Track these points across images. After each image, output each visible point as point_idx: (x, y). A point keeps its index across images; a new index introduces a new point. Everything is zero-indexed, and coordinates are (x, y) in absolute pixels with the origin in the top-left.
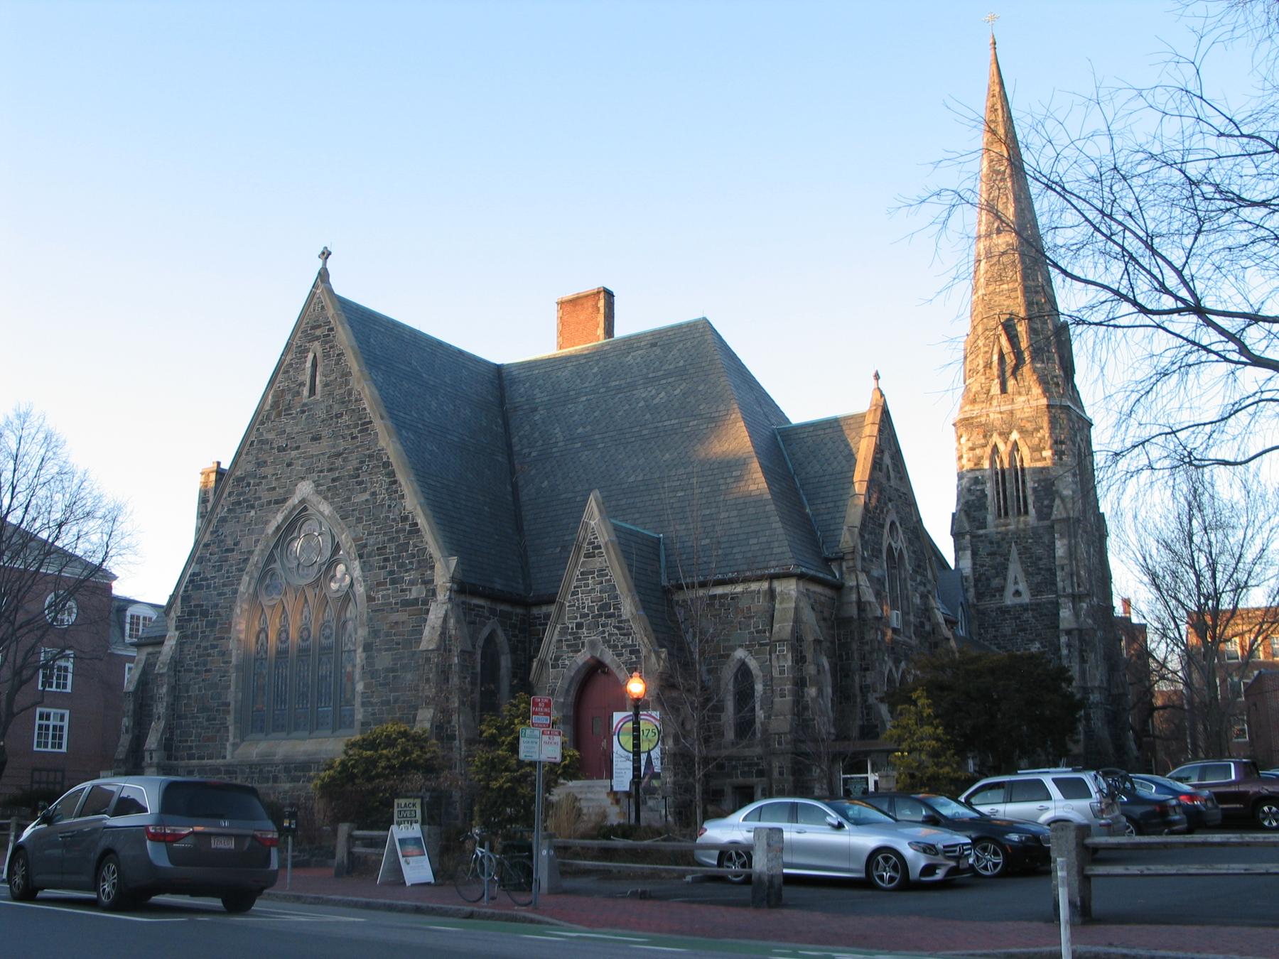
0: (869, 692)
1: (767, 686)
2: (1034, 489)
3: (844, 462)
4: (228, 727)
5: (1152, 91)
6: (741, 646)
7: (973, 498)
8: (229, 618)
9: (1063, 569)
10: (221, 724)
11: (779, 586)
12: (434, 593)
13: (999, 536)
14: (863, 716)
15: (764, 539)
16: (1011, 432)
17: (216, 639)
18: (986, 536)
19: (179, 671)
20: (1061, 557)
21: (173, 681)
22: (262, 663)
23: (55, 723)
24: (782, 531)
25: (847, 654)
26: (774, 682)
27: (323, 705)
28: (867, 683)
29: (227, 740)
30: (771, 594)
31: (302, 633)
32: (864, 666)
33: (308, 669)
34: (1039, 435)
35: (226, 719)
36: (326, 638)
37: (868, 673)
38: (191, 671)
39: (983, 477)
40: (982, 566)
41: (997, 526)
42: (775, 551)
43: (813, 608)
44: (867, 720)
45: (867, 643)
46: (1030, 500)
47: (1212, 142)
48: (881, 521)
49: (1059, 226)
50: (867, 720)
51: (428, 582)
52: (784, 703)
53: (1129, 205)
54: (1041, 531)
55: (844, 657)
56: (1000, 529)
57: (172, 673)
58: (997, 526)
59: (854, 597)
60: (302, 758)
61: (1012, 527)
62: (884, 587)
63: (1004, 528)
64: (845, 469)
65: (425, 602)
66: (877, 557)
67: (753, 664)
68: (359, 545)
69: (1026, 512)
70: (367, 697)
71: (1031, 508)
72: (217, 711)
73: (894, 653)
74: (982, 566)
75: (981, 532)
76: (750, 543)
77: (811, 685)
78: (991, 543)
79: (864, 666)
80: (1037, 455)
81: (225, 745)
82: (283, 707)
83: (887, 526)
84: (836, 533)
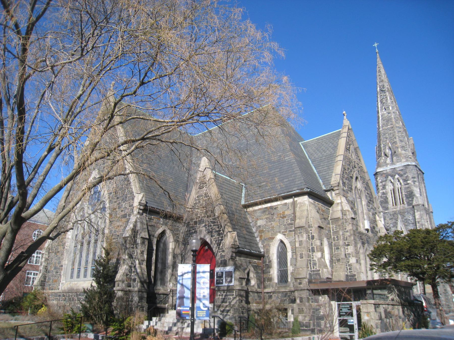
0: (350, 257)
1: (294, 253)
2: (405, 195)
3: (332, 150)
6: (280, 232)
7: (382, 199)
9: (419, 223)
11: (299, 200)
13: (393, 212)
14: (347, 270)
15: (291, 179)
16: (395, 175)
18: (389, 213)
20: (418, 219)
21: (47, 257)
23: (31, 276)
24: (300, 174)
25: (337, 237)
26: (297, 250)
28: (349, 252)
29: (61, 282)
30: (294, 203)
32: (346, 244)
34: (406, 175)
37: (349, 247)
39: (386, 192)
40: (388, 223)
41: (393, 209)
42: (297, 183)
43: (318, 212)
44: (350, 272)
45: (347, 231)
46: (404, 199)
48: (351, 175)
50: (350, 272)
51: (131, 206)
52: (301, 263)
54: (409, 210)
55: (336, 239)
56: (393, 210)
57: (47, 253)
58: (393, 209)
59: (339, 208)
61: (398, 209)
62: (355, 206)
63: (395, 209)
64: (333, 153)
66: (351, 192)
67: (286, 242)
69: (403, 203)
71: (405, 201)
73: (362, 239)
74: (388, 223)
75: (386, 211)
76: (284, 181)
77: (318, 251)
78: (391, 215)
79: (346, 244)
80: (405, 183)
83: (354, 178)
84: (329, 179)
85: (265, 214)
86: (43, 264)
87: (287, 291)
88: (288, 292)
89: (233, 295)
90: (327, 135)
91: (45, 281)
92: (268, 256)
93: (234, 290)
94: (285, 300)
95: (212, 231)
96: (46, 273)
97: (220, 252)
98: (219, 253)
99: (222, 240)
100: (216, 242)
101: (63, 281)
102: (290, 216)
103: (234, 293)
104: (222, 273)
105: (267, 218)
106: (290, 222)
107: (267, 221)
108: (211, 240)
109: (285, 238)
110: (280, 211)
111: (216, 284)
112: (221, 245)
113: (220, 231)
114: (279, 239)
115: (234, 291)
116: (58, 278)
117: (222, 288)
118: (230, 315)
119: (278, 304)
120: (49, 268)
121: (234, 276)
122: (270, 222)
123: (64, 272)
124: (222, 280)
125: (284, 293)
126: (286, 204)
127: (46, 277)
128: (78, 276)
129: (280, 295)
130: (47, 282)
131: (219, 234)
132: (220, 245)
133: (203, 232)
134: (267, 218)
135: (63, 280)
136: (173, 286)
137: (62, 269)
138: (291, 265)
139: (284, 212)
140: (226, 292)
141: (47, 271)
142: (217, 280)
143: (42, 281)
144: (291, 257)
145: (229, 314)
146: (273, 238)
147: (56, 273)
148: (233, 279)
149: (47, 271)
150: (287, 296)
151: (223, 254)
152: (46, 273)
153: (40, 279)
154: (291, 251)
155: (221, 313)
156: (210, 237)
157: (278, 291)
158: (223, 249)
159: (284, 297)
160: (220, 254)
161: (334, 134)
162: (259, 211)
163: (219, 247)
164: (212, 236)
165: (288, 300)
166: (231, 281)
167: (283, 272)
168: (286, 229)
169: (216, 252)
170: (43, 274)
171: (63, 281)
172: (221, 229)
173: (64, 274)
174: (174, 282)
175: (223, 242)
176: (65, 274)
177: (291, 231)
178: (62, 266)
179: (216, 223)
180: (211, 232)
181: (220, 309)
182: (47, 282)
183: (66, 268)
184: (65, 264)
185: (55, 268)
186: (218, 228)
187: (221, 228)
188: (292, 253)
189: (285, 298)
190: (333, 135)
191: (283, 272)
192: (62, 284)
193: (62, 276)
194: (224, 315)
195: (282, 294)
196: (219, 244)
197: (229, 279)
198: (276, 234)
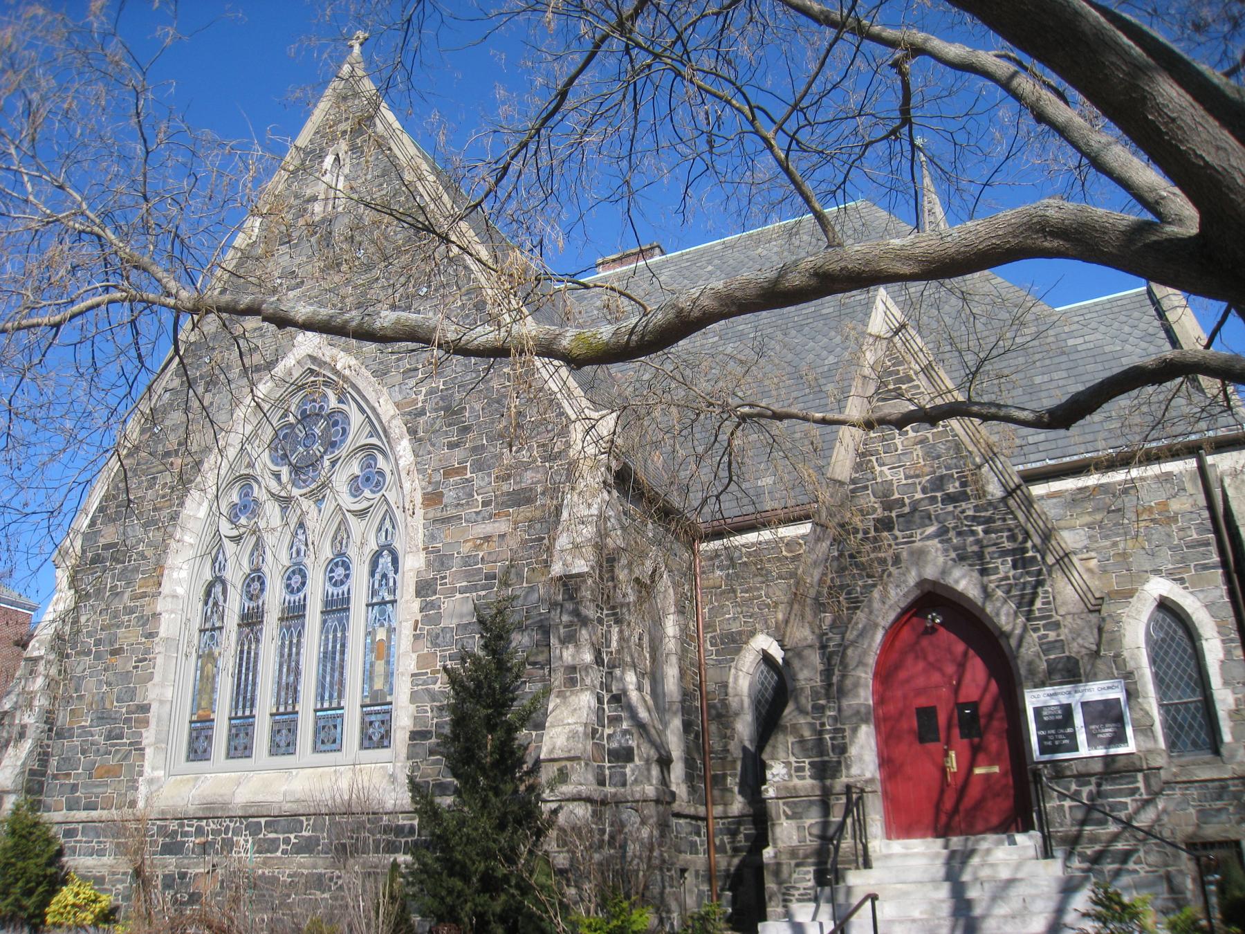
4: (143, 749)
5: (970, 359)
6: (1157, 572)
8: (159, 568)
10: (131, 744)
12: (571, 470)
17: (134, 598)
19: (68, 656)
22: (212, 636)
27: (326, 705)
29: (141, 774)
31: (289, 578)
33: (290, 649)
35: (141, 735)
36: (335, 585)
38: (88, 653)
47: (148, 590)
49: (617, 295)
53: (56, 522)
60: (288, 808)
65: (554, 491)
68: (410, 413)
70: (425, 683)
72: (127, 720)
81: (136, 781)
82: (247, 713)
85: (1079, 510)
86: (36, 703)
87: (1226, 776)
88: (1230, 782)
89: (1134, 791)
90: (1096, 304)
91: (44, 774)
92: (1117, 656)
93: (1141, 770)
94: (1219, 810)
95: (983, 552)
96: (49, 738)
97: (1036, 630)
98: (1035, 635)
99: (1040, 583)
100: (1008, 592)
101: (153, 769)
102: (1194, 516)
103: (1141, 785)
104: (1067, 710)
105: (1090, 526)
106: (1195, 536)
107: (1092, 532)
108: (984, 589)
109: (1182, 592)
110: (1151, 498)
111: (1042, 752)
112: (1038, 604)
113: (1025, 550)
114: (1156, 595)
115: (1140, 776)
116: (126, 757)
117: (1075, 768)
118: (1135, 871)
119: (1190, 829)
120: (63, 719)
121: (1133, 720)
122: (1106, 537)
123: (158, 733)
124: (1073, 736)
125: (1210, 785)
126: (1168, 477)
127: (46, 754)
128: (283, 741)
129: (1194, 792)
130: (55, 777)
131: (1021, 562)
132: (1032, 603)
133: (930, 558)
134: (1090, 526)
135: (152, 766)
136: (790, 776)
137: (146, 723)
138: (1226, 683)
139: (1165, 504)
140: (1093, 780)
141: (50, 730)
142: (1041, 739)
143: (32, 773)
144: (1221, 656)
145: (1131, 865)
146: (1130, 594)
147: (109, 737)
148: (1129, 731)
149: (50, 730)
150: (1225, 797)
151: (1052, 635)
152: (49, 738)
153: (24, 764)
154: (1216, 634)
155: (1085, 865)
156: (976, 574)
157: (1185, 779)
158: (1050, 617)
159: (1213, 800)
160: (1040, 638)
161: (1124, 302)
162: (1054, 500)
163: (1030, 612)
164: (984, 572)
165: (1231, 809)
166: (1119, 738)
167: (1178, 711)
168: (1183, 560)
169: (1018, 631)
170: (39, 744)
171: (153, 769)
172: (1029, 544)
173: (158, 741)
174: (792, 759)
175: (1046, 592)
176: (163, 741)
177: (1205, 567)
178: (145, 709)
179: (999, 523)
180: (980, 556)
181: (1079, 849)
182: (55, 777)
183: (165, 716)
184: (162, 702)
185: (103, 717)
186: (1012, 538)
187: (1025, 541)
188: (1223, 641)
189: (1219, 804)
190: (1119, 303)
191: (1178, 711)
192: (151, 781)
193: (149, 752)
194: (1101, 872)
195: (1201, 787)
196: (1026, 602)
197: (1108, 731)
198: (1140, 577)
